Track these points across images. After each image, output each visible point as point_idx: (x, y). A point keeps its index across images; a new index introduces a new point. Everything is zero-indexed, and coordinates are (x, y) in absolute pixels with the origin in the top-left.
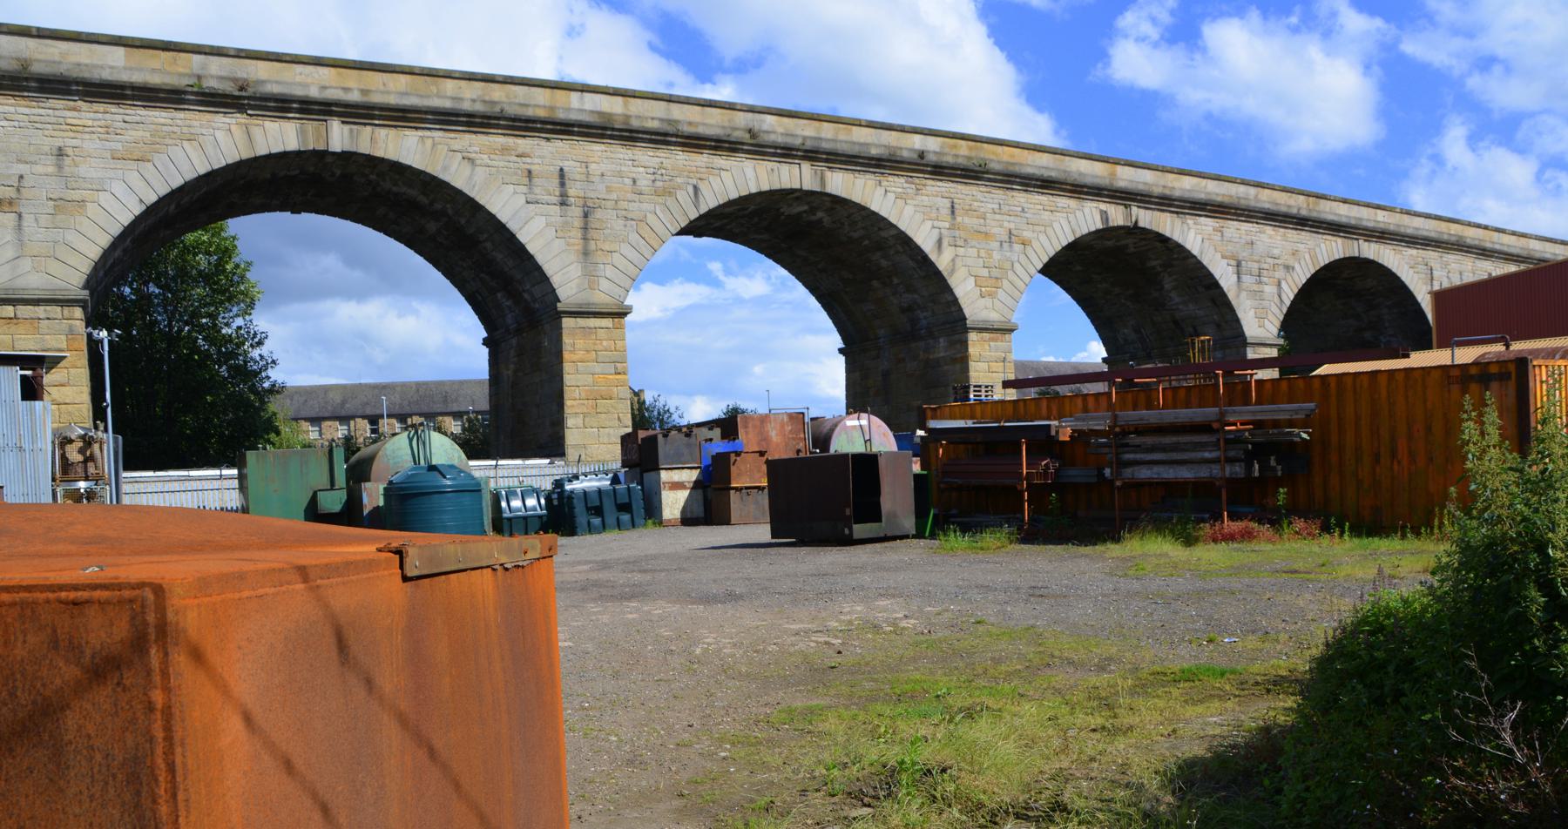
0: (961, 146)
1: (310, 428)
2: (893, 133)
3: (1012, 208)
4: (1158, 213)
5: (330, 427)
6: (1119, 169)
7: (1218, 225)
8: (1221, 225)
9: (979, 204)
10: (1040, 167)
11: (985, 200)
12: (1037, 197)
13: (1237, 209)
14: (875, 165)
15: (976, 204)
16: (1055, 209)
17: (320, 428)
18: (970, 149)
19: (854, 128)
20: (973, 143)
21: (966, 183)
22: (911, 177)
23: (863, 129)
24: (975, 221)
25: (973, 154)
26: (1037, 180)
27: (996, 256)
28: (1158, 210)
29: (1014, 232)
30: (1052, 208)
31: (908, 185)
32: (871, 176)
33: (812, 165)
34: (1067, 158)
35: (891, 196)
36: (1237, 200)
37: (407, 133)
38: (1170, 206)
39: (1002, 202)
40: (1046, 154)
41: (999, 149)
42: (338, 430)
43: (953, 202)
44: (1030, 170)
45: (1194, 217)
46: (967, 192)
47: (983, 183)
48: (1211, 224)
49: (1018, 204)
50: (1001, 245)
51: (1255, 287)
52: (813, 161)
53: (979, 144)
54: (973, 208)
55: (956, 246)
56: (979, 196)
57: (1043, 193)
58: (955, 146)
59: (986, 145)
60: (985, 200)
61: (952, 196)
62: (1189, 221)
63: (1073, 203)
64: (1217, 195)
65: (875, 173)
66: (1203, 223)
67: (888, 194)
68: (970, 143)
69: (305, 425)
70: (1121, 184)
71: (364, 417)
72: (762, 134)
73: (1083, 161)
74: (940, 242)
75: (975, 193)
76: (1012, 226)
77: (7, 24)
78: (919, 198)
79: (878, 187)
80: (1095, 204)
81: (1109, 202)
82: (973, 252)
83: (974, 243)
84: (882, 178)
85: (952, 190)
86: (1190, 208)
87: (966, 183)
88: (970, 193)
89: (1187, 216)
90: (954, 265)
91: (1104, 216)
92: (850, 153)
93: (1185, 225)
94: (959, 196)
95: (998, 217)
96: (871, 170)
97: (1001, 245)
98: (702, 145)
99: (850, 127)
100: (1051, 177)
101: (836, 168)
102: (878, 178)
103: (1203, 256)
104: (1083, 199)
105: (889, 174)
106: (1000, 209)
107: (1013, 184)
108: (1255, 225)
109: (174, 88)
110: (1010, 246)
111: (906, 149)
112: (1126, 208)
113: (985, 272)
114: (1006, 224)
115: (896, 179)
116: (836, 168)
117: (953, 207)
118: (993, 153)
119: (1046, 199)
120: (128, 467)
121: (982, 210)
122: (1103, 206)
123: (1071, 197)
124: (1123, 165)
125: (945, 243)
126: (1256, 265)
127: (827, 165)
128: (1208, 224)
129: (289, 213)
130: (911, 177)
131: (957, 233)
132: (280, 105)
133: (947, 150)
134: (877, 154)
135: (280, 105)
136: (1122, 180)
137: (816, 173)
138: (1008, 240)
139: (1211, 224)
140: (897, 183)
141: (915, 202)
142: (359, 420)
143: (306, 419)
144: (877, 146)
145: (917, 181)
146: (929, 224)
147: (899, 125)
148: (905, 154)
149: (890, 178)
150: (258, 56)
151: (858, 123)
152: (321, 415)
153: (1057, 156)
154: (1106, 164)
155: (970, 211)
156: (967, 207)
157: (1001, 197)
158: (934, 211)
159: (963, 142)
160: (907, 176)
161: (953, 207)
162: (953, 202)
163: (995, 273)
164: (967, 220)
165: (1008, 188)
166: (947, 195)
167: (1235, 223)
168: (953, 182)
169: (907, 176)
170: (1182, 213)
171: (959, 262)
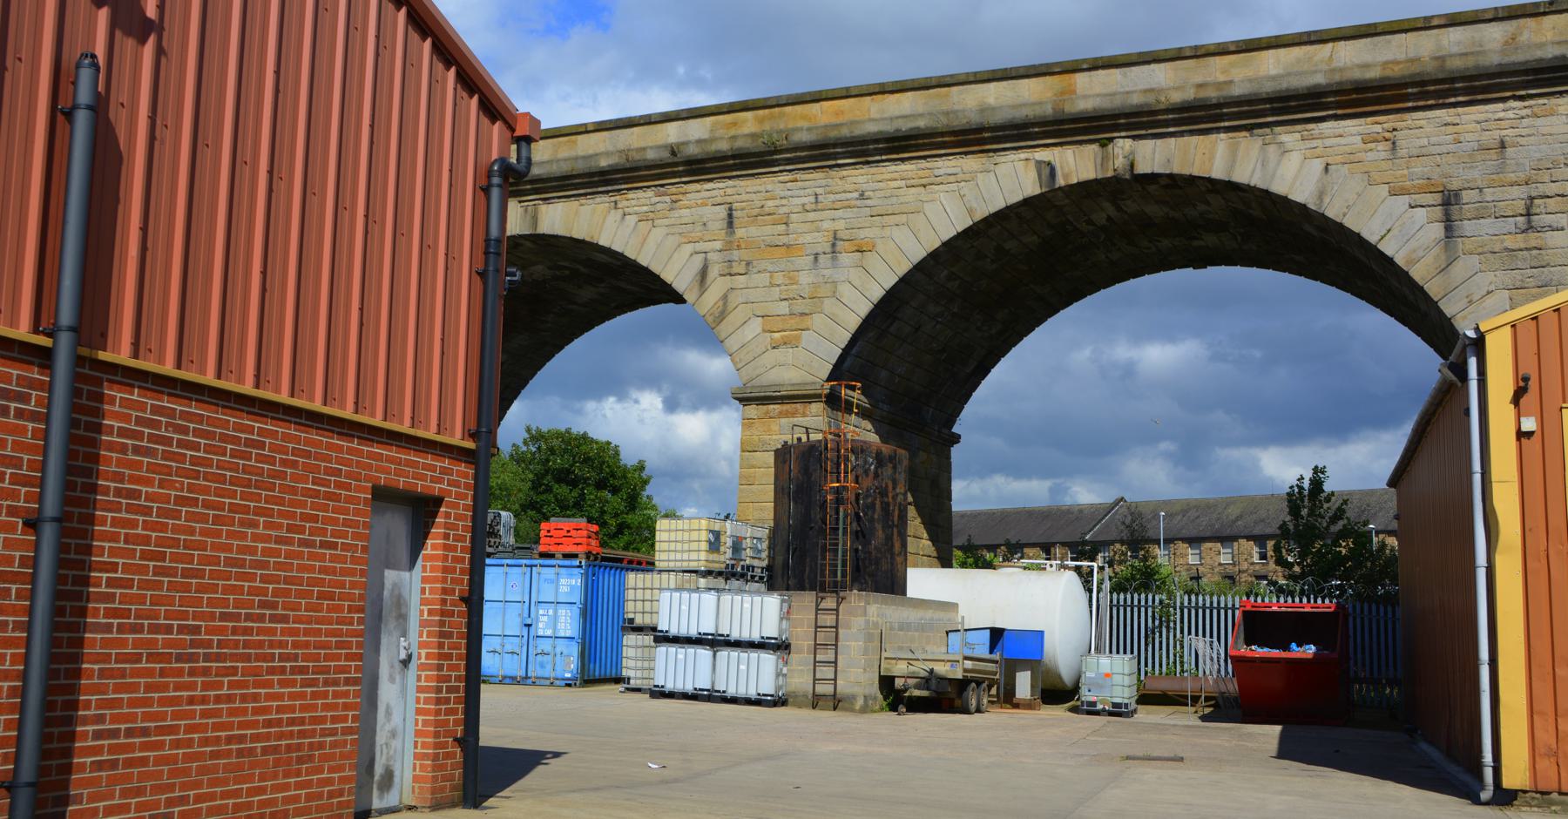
0: (745, 121)
1: (1190, 551)
2: (636, 129)
3: (838, 197)
4: (1195, 139)
5: (1211, 549)
6: (1081, 80)
7: (1378, 128)
8: (1388, 126)
9: (777, 202)
10: (891, 119)
11: (790, 193)
12: (893, 168)
13: (1423, 83)
14: (600, 181)
15: (770, 203)
16: (932, 180)
17: (1200, 550)
18: (761, 121)
19: (580, 137)
20: (767, 111)
21: (753, 175)
22: (662, 186)
23: (592, 135)
24: (769, 229)
25: (767, 127)
26: (876, 141)
27: (805, 278)
28: (1192, 133)
29: (840, 235)
30: (924, 181)
31: (658, 199)
32: (605, 198)
33: (520, 202)
34: (955, 89)
35: (631, 220)
36: (1435, 64)
37: (845, 173)
38: (1221, 118)
39: (819, 191)
40: (909, 94)
41: (815, 107)
42: (1220, 554)
43: (731, 209)
44: (872, 128)
45: (1299, 127)
46: (756, 189)
47: (781, 168)
48: (1354, 130)
49: (851, 187)
50: (816, 259)
51: (1518, 241)
52: (521, 196)
53: (777, 109)
54: (766, 210)
55: (731, 275)
56: (779, 190)
57: (903, 160)
58: (735, 124)
59: (788, 109)
60: (790, 193)
61: (729, 199)
62: (1284, 138)
63: (971, 163)
64: (1366, 66)
65: (608, 192)
66: (1327, 132)
67: (627, 217)
68: (761, 112)
69: (1182, 546)
70: (1084, 105)
71: (1249, 538)
72: (682, 148)
73: (993, 85)
74: (703, 273)
75: (769, 187)
76: (840, 225)
77: (809, 93)
78: (676, 214)
79: (613, 211)
80: (1023, 155)
81: (1061, 144)
82: (762, 279)
83: (764, 265)
84: (618, 198)
85: (729, 191)
86: (1274, 112)
87: (753, 175)
88: (760, 188)
89: (1278, 129)
90: (725, 304)
91: (1046, 171)
92: (558, 174)
93: (1272, 149)
94: (744, 197)
95: (812, 216)
96: (600, 189)
97: (816, 259)
98: (568, 185)
99: (573, 137)
100: (918, 128)
101: (553, 198)
102: (613, 199)
103: (1327, 200)
104: (995, 151)
105: (628, 189)
106: (817, 202)
107: (836, 159)
108: (1512, 104)
109: (1071, 117)
110: (834, 259)
111: (651, 148)
112: (1103, 146)
113: (784, 308)
114: (826, 225)
115: (640, 194)
116: (553, 198)
117: (730, 216)
118: (804, 117)
119: (913, 167)
120: (904, 592)
121: (783, 210)
122: (1043, 155)
123: (966, 153)
124: (1089, 70)
125: (714, 272)
126: (1519, 192)
127: (538, 196)
128: (1347, 133)
129: (1191, 269)
130: (662, 186)
131: (736, 255)
132: (891, 145)
133: (720, 132)
134: (609, 166)
135: (891, 145)
136: (1085, 97)
137: (526, 211)
138: (828, 250)
139: (1354, 130)
140: (641, 199)
141: (666, 222)
142: (1243, 541)
143: (1184, 540)
144: (607, 154)
145: (673, 189)
146: (689, 248)
147: (641, 117)
148: (651, 155)
149: (631, 195)
150: (698, 113)
151: (583, 129)
152: (1202, 535)
153: (931, 91)
154: (1048, 79)
155: (760, 215)
156: (756, 211)
157: (824, 182)
158: (699, 227)
159: (748, 115)
160: (655, 186)
161: (730, 216)
162: (731, 209)
163: (800, 306)
164: (754, 231)
165: (830, 167)
166: (719, 200)
167: (1438, 113)
168: (730, 178)
169: (655, 186)
170: (1261, 126)
171: (735, 299)
